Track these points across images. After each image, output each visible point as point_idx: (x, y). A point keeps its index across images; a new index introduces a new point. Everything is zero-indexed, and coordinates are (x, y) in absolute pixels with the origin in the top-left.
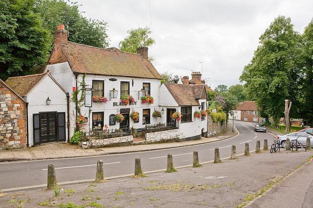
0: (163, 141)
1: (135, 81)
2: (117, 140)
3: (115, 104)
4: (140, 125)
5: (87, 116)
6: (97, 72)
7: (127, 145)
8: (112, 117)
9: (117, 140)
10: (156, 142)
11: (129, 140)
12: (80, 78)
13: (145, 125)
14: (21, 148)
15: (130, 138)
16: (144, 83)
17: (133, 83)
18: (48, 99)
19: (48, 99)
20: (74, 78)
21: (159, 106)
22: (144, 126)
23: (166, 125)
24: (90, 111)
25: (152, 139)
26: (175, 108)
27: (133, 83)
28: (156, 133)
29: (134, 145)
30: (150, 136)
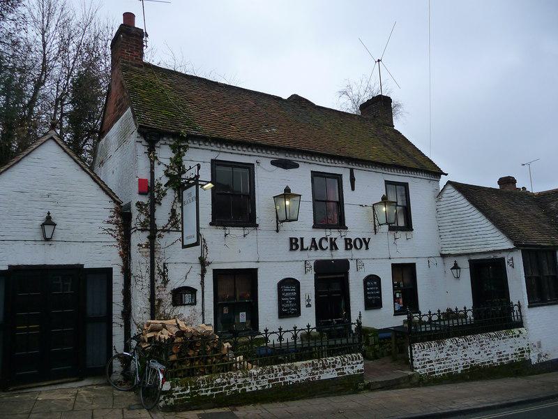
0: (475, 373)
1: (362, 175)
2: (302, 372)
3: (295, 244)
4: (386, 318)
5: (194, 282)
6: (357, 155)
7: (339, 393)
8: (287, 288)
9: (302, 372)
10: (451, 378)
11: (348, 370)
12: (165, 154)
13: (405, 317)
14: (303, 349)
15: (354, 365)
16: (387, 183)
17: (352, 180)
18: (49, 221)
19: (49, 221)
20: (142, 149)
21: (443, 256)
22: (400, 321)
23: (470, 314)
24: (203, 262)
25: (436, 367)
26: (499, 256)
27: (352, 180)
28: (448, 342)
29: (369, 388)
30: (426, 357)
